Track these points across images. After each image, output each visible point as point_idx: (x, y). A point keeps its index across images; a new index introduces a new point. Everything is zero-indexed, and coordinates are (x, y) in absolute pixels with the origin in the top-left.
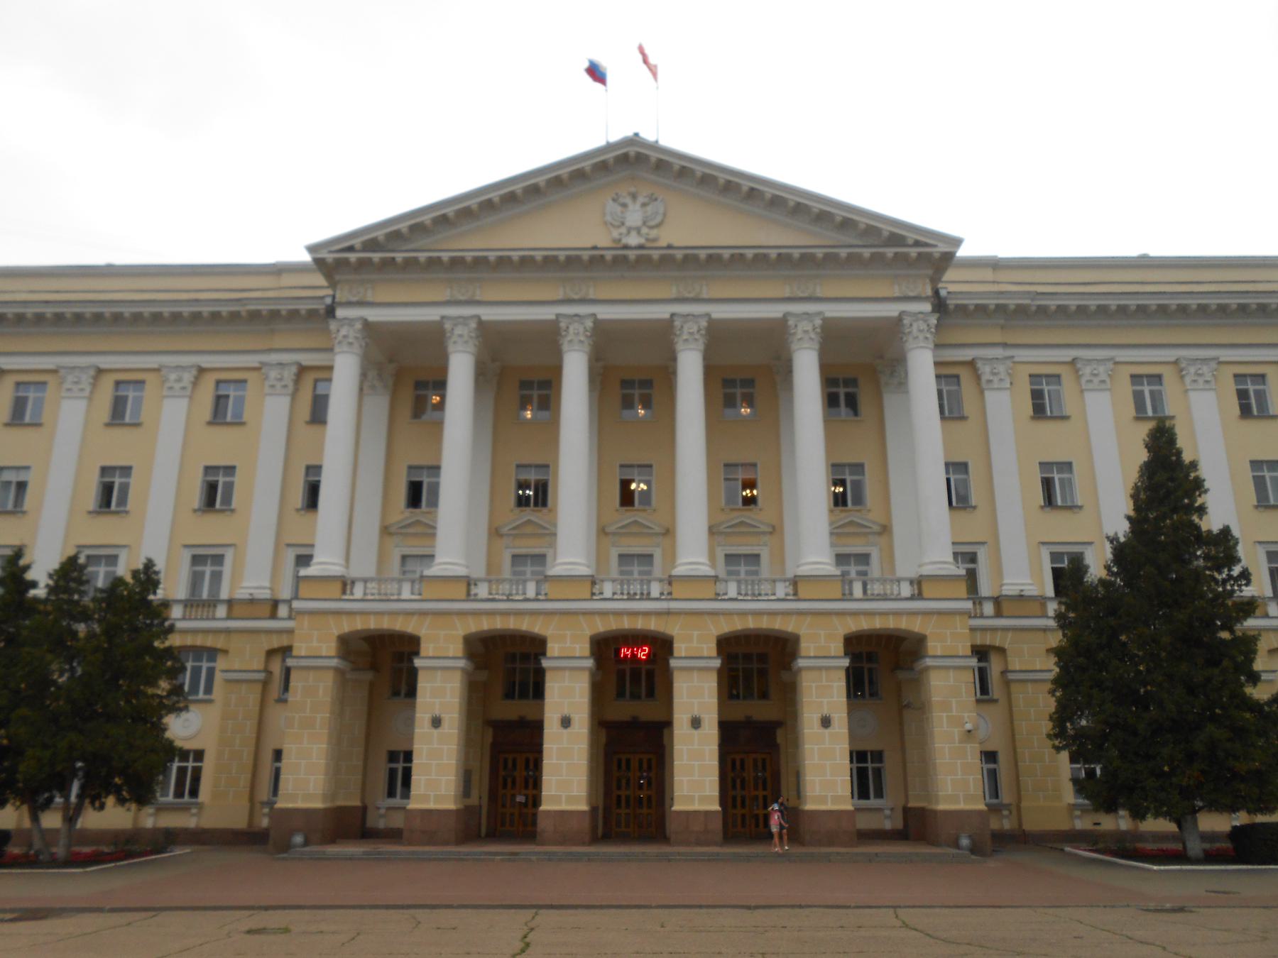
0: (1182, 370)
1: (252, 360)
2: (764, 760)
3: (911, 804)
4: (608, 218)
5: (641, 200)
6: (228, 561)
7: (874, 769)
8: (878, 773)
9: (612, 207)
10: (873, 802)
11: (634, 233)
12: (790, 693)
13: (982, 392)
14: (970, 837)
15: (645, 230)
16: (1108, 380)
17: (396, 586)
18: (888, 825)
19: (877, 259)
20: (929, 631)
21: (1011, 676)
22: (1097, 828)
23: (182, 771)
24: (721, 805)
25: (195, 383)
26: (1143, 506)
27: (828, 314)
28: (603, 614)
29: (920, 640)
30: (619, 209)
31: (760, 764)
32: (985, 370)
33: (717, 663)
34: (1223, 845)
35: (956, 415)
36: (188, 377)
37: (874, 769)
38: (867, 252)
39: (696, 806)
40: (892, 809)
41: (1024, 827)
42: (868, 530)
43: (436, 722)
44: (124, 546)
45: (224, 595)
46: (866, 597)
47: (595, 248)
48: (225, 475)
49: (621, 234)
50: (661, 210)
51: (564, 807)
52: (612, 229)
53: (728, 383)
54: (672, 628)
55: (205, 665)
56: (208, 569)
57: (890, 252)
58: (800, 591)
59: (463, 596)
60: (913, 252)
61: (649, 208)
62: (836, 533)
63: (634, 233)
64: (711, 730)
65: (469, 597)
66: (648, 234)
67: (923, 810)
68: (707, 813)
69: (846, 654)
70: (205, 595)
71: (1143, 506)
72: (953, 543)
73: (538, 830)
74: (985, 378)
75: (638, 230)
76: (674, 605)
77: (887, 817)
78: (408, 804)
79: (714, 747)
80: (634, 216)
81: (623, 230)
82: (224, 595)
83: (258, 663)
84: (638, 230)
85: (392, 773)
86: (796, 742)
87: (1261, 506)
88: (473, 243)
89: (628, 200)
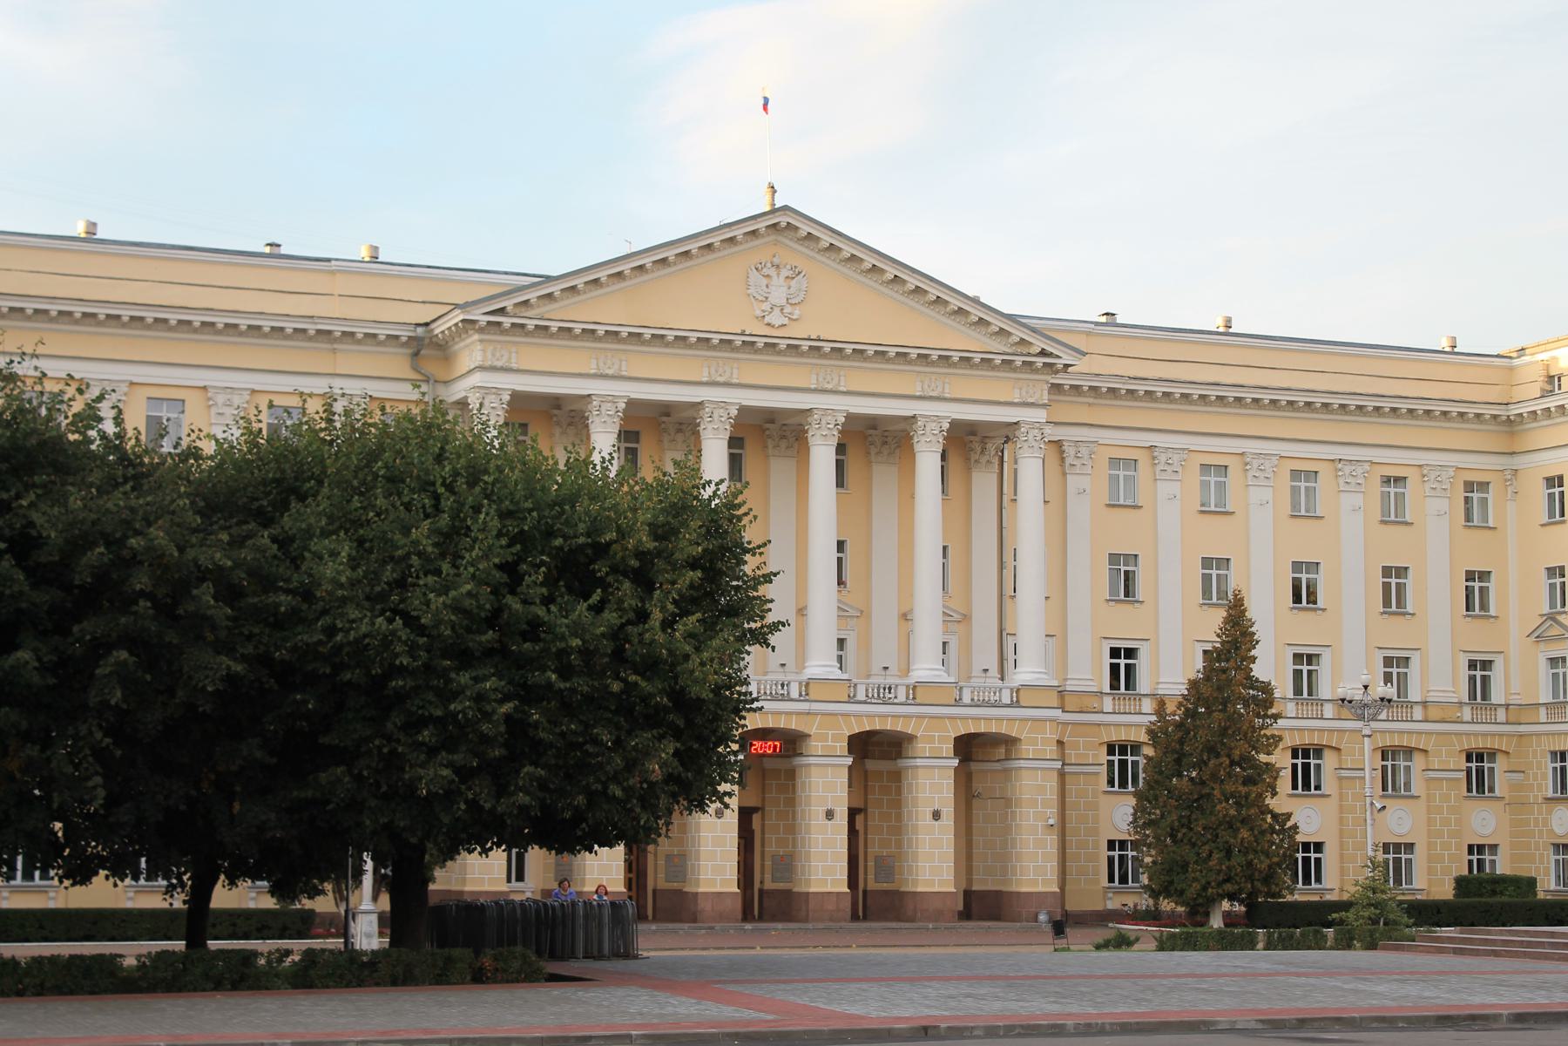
0: (1154, 458)
3: (975, 888)
5: (785, 272)
6: (1498, 667)
7: (1315, 859)
11: (777, 311)
13: (1064, 474)
14: (1049, 913)
15: (788, 309)
16: (1180, 469)
20: (814, 731)
23: (1306, 861)
24: (849, 888)
26: (283, 609)
27: (853, 410)
28: (964, 718)
29: (911, 738)
30: (765, 281)
32: (1070, 451)
33: (956, 762)
35: (1129, 502)
37: (1315, 859)
38: (1019, 360)
41: (1068, 908)
43: (936, 815)
46: (1426, 721)
47: (819, 340)
48: (1481, 580)
49: (763, 311)
51: (829, 889)
52: (755, 303)
54: (811, 728)
55: (1402, 764)
57: (1040, 361)
58: (918, 696)
59: (846, 699)
61: (793, 283)
63: (777, 311)
65: (851, 700)
67: (998, 893)
68: (838, 894)
69: (850, 751)
71: (283, 609)
73: (699, 908)
74: (1068, 461)
78: (684, 887)
81: (766, 306)
88: (1023, 321)
89: (773, 272)
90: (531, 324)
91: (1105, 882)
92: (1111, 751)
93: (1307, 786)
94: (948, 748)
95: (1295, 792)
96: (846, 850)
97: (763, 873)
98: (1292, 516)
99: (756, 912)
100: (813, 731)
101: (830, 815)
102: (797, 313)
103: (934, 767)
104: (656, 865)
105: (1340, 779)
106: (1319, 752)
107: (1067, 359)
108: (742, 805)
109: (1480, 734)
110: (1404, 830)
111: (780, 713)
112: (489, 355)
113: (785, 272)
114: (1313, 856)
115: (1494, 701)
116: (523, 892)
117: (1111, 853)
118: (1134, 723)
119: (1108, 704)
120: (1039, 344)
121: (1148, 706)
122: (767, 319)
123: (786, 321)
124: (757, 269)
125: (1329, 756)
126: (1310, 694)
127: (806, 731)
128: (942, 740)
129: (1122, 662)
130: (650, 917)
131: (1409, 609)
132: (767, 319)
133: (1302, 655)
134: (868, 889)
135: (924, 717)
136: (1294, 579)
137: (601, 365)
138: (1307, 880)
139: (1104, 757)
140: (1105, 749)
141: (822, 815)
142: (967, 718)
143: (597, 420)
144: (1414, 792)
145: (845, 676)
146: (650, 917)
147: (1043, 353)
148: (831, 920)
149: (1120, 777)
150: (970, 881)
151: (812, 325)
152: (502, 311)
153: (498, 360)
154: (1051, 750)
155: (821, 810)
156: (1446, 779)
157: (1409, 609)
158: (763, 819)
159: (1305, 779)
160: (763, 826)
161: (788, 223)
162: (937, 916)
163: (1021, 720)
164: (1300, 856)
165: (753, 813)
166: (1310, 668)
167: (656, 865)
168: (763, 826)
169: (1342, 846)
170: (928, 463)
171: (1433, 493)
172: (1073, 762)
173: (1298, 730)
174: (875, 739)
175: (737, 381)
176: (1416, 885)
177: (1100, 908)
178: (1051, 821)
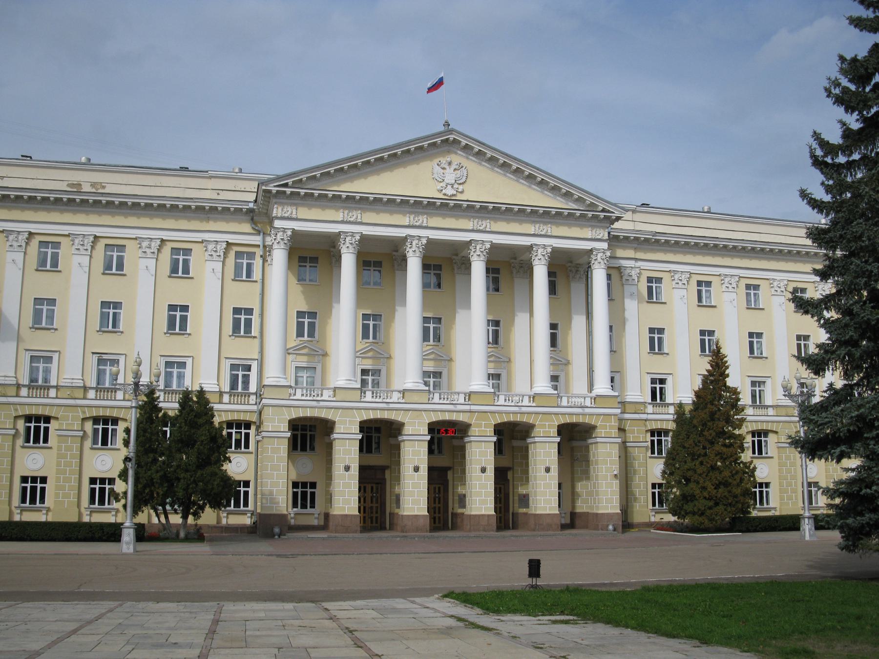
1: (66, 230)
2: (439, 488)
4: (436, 176)
5: (454, 166)
7: (41, 488)
8: (313, 495)
9: (437, 169)
10: (309, 510)
12: (396, 449)
15: (456, 186)
17: (583, 400)
18: (315, 522)
19: (595, 217)
21: (628, 444)
22: (662, 520)
23: (761, 492)
24: (428, 512)
25: (93, 247)
27: (555, 245)
29: (593, 428)
30: (442, 171)
31: (437, 490)
34: (217, 534)
36: (155, 245)
37: (41, 488)
38: (590, 214)
39: (609, 511)
40: (319, 514)
42: (501, 360)
44: (56, 351)
45: (53, 383)
49: (442, 187)
50: (465, 174)
51: (416, 513)
53: (302, 259)
56: (175, 371)
57: (602, 215)
60: (602, 215)
62: (359, 355)
63: (449, 187)
64: (355, 471)
66: (458, 188)
68: (489, 516)
70: (107, 385)
72: (611, 372)
75: (452, 185)
76: (474, 408)
77: (316, 518)
79: (425, 482)
80: (450, 176)
82: (53, 383)
83: (77, 425)
84: (452, 185)
85: (24, 490)
86: (398, 479)
87: (651, 353)
89: (446, 166)
90: (330, 194)
91: (650, 506)
92: (652, 435)
93: (37, 440)
94: (554, 431)
95: (754, 455)
96: (493, 490)
97: (453, 504)
98: (748, 308)
99: (511, 525)
100: (406, 421)
101: (483, 470)
102: (461, 188)
103: (482, 441)
104: (453, 499)
105: (778, 448)
106: (47, 419)
107: (617, 214)
108: (430, 465)
109: (36, 404)
110: (765, 475)
111: (593, 415)
112: (346, 215)
113: (454, 166)
114: (309, 490)
115: (667, 401)
116: (314, 514)
117: (654, 490)
118: (666, 418)
119: (650, 409)
120: (601, 206)
121: (671, 410)
122: (444, 191)
123: (455, 192)
124: (438, 165)
125: (53, 426)
126: (760, 403)
127: (334, 419)
128: (550, 426)
129: (658, 386)
130: (450, 528)
131: (666, 351)
132: (444, 191)
133: (756, 382)
134: (515, 512)
135: (540, 414)
136: (701, 340)
137: (346, 215)
138: (761, 503)
139: (649, 438)
140: (649, 434)
141: (412, 469)
142: (565, 414)
143: (411, 250)
144: (769, 455)
145: (616, 394)
146: (450, 528)
147: (603, 210)
148: (484, 530)
149: (655, 448)
150: (574, 507)
151: (472, 193)
152: (286, 185)
153: (416, 222)
154: (615, 432)
155: (342, 466)
156: (609, 443)
157: (666, 351)
158: (513, 474)
159: (759, 448)
160: (513, 477)
161: (454, 138)
162: (549, 527)
163: (597, 415)
164: (242, 489)
165: (448, 470)
166: (760, 389)
167: (453, 499)
168: (513, 477)
169: (781, 484)
170: (478, 269)
171: (77, 252)
172: (631, 440)
173: (755, 422)
174: (517, 428)
175: (550, 234)
176: (772, 505)
177: (647, 521)
178: (615, 473)
